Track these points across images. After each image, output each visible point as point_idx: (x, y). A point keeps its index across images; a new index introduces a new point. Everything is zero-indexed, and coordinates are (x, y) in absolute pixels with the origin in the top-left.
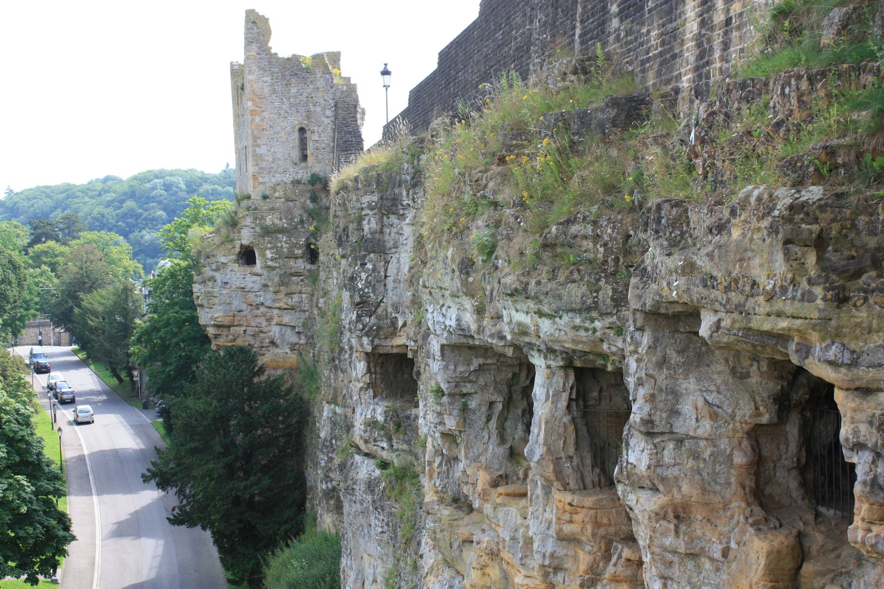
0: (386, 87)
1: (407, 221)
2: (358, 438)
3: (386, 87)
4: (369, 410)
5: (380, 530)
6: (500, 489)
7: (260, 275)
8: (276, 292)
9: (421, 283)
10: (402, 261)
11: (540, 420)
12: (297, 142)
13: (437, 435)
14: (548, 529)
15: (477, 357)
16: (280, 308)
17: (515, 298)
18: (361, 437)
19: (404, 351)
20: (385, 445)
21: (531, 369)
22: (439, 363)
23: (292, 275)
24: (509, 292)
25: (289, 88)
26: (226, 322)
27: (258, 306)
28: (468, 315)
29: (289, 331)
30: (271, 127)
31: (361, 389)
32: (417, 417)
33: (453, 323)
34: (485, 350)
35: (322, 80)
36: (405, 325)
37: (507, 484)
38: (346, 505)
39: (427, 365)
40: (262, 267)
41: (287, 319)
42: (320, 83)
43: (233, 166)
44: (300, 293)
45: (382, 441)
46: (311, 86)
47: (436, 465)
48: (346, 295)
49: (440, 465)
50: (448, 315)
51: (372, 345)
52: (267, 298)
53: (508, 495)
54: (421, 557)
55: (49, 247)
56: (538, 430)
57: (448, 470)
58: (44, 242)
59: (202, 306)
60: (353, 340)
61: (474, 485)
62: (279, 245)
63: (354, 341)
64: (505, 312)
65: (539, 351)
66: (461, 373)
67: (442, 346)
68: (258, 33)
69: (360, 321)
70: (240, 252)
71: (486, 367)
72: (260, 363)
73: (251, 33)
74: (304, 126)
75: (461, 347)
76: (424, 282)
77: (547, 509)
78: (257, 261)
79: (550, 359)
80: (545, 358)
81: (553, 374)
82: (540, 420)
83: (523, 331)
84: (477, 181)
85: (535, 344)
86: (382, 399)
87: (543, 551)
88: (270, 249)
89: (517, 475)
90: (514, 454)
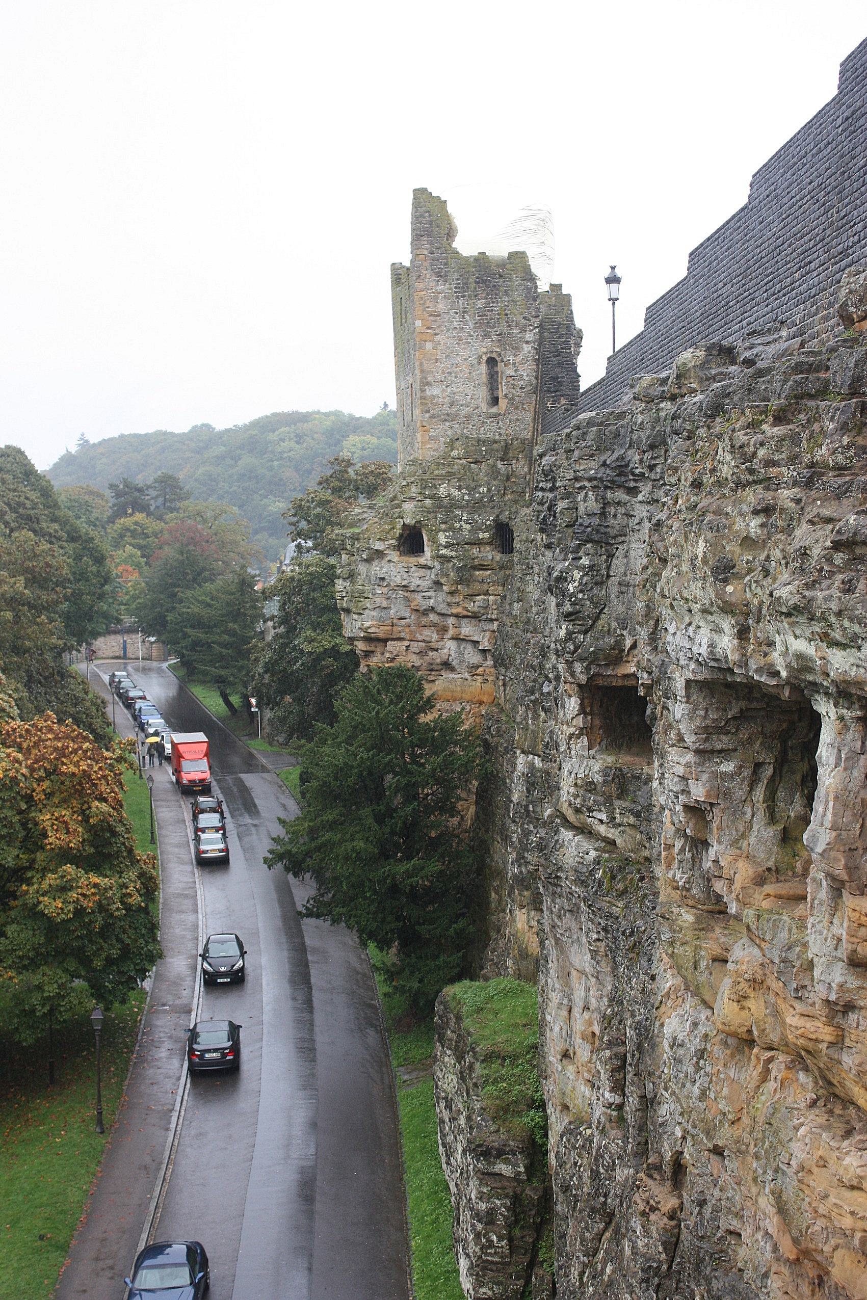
0: (613, 300)
1: (640, 497)
2: (566, 805)
3: (613, 300)
4: (581, 764)
5: (595, 936)
6: (768, 889)
7: (430, 568)
8: (452, 593)
9: (658, 590)
10: (632, 554)
11: (828, 794)
12: (484, 378)
13: (678, 808)
14: (836, 949)
15: (738, 699)
16: (457, 616)
17: (793, 619)
18: (570, 804)
19: (634, 683)
20: (603, 817)
21: (815, 721)
22: (683, 706)
23: (475, 568)
24: (785, 610)
25: (462, 287)
26: (381, 632)
27: (425, 613)
28: (726, 639)
29: (469, 648)
31: (571, 736)
32: (650, 779)
33: (704, 650)
34: (750, 689)
36: (634, 646)
37: (778, 881)
38: (547, 901)
39: (665, 707)
40: (432, 557)
41: (467, 629)
42: (518, 295)
43: (393, 406)
44: (487, 593)
45: (600, 811)
46: (505, 298)
47: (676, 850)
48: (552, 601)
49: (682, 850)
50: (696, 640)
51: (588, 673)
52: (438, 600)
53: (779, 897)
54: (653, 978)
55: (136, 523)
56: (824, 810)
57: (693, 858)
58: (131, 515)
59: (348, 611)
60: (560, 666)
61: (731, 881)
62: (457, 525)
63: (561, 667)
64: (777, 639)
65: (827, 694)
66: (714, 721)
67: (688, 682)
68: (431, 223)
69: (570, 639)
70: (401, 535)
71: (750, 714)
72: (427, 693)
73: (421, 223)
74: (494, 355)
75: (720, 686)
76: (662, 589)
77: (835, 921)
78: (426, 548)
79: (843, 707)
80: (836, 705)
81: (846, 728)
82: (828, 794)
83: (803, 664)
84: (741, 447)
85: (821, 684)
86: (601, 751)
87: (828, 981)
88: (444, 531)
89: (793, 868)
90: (789, 837)
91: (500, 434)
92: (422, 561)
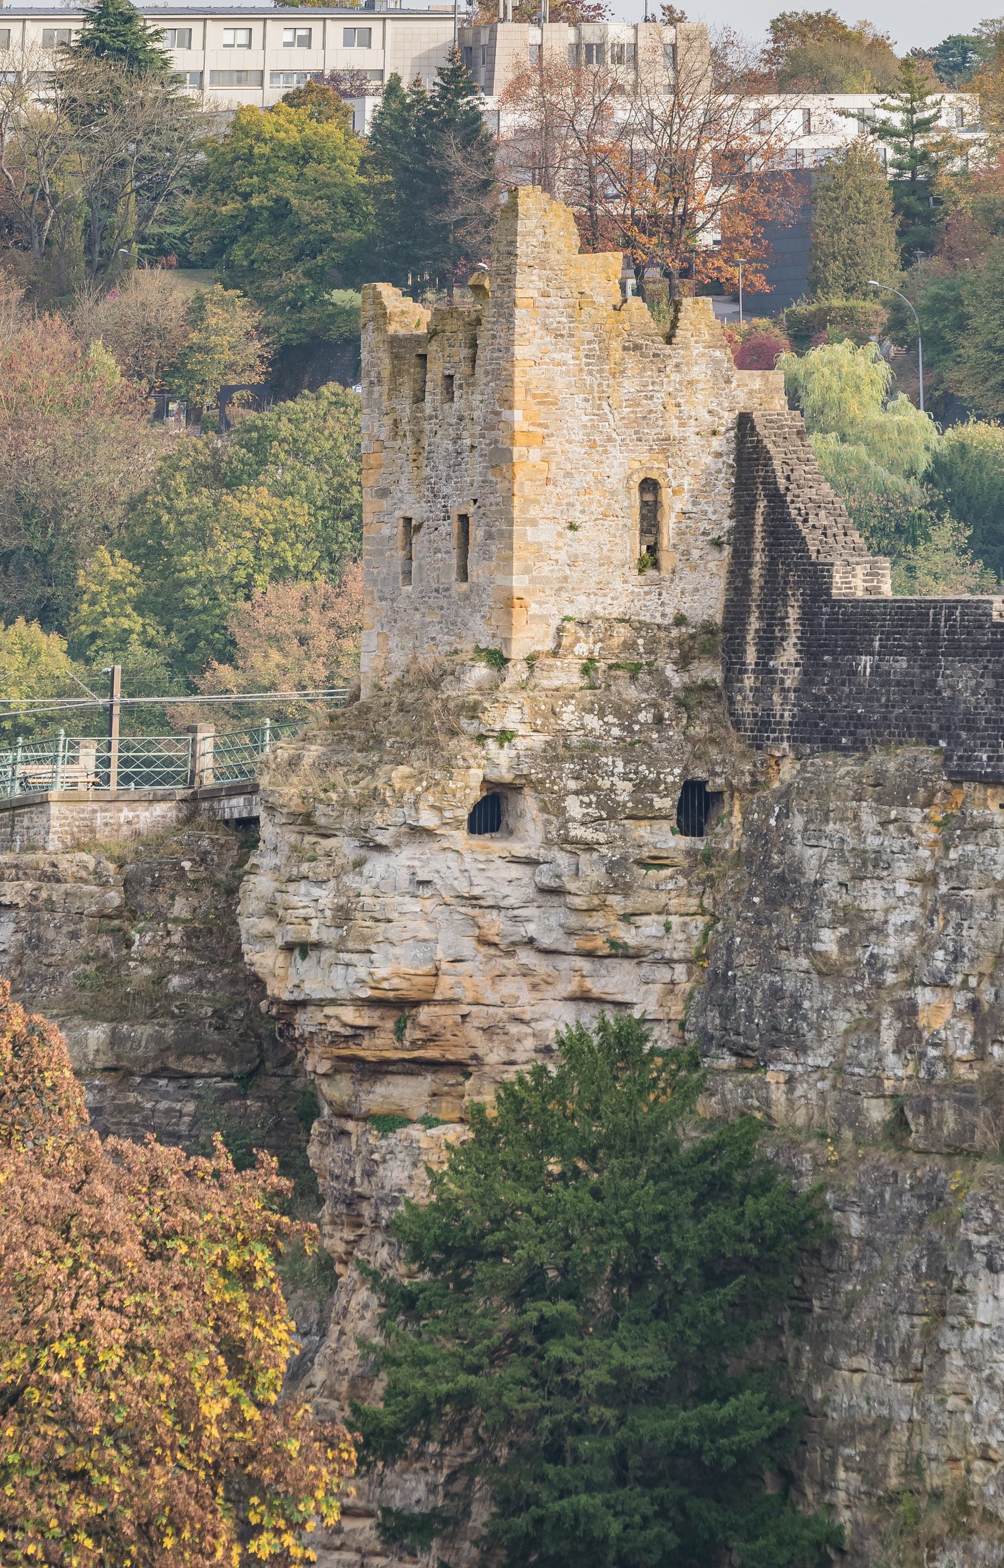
12: (634, 520)
30: (568, 475)
35: (703, 361)
40: (548, 843)
46: (676, 377)
62: (605, 783)
74: (654, 475)
88: (577, 793)
91: (663, 615)
92: (519, 849)
